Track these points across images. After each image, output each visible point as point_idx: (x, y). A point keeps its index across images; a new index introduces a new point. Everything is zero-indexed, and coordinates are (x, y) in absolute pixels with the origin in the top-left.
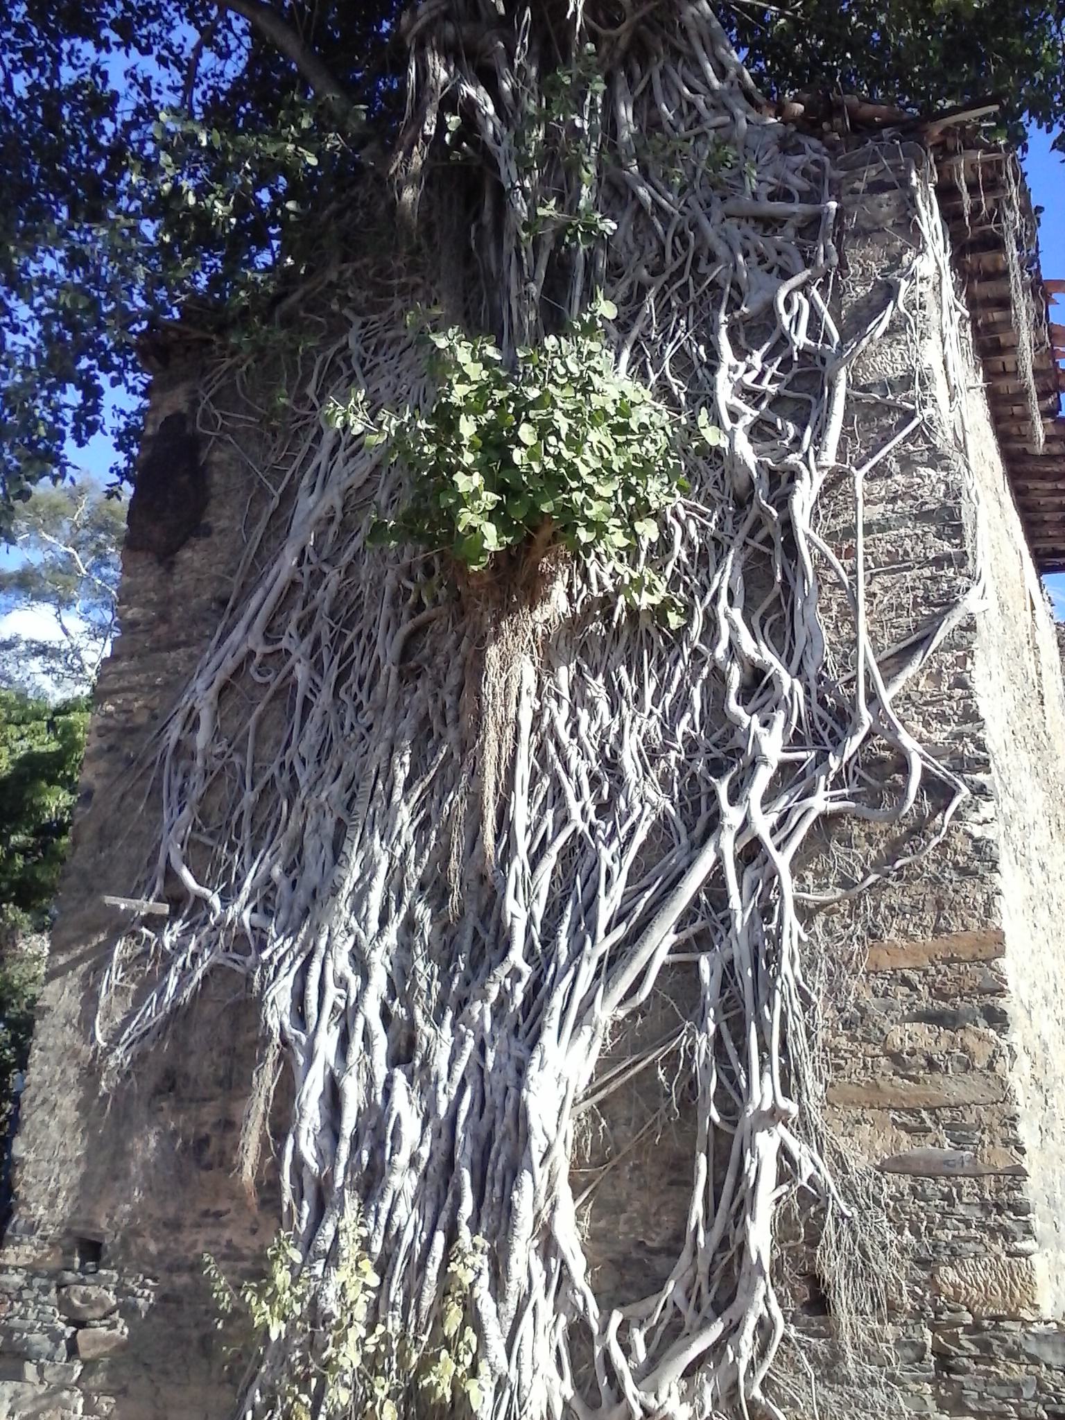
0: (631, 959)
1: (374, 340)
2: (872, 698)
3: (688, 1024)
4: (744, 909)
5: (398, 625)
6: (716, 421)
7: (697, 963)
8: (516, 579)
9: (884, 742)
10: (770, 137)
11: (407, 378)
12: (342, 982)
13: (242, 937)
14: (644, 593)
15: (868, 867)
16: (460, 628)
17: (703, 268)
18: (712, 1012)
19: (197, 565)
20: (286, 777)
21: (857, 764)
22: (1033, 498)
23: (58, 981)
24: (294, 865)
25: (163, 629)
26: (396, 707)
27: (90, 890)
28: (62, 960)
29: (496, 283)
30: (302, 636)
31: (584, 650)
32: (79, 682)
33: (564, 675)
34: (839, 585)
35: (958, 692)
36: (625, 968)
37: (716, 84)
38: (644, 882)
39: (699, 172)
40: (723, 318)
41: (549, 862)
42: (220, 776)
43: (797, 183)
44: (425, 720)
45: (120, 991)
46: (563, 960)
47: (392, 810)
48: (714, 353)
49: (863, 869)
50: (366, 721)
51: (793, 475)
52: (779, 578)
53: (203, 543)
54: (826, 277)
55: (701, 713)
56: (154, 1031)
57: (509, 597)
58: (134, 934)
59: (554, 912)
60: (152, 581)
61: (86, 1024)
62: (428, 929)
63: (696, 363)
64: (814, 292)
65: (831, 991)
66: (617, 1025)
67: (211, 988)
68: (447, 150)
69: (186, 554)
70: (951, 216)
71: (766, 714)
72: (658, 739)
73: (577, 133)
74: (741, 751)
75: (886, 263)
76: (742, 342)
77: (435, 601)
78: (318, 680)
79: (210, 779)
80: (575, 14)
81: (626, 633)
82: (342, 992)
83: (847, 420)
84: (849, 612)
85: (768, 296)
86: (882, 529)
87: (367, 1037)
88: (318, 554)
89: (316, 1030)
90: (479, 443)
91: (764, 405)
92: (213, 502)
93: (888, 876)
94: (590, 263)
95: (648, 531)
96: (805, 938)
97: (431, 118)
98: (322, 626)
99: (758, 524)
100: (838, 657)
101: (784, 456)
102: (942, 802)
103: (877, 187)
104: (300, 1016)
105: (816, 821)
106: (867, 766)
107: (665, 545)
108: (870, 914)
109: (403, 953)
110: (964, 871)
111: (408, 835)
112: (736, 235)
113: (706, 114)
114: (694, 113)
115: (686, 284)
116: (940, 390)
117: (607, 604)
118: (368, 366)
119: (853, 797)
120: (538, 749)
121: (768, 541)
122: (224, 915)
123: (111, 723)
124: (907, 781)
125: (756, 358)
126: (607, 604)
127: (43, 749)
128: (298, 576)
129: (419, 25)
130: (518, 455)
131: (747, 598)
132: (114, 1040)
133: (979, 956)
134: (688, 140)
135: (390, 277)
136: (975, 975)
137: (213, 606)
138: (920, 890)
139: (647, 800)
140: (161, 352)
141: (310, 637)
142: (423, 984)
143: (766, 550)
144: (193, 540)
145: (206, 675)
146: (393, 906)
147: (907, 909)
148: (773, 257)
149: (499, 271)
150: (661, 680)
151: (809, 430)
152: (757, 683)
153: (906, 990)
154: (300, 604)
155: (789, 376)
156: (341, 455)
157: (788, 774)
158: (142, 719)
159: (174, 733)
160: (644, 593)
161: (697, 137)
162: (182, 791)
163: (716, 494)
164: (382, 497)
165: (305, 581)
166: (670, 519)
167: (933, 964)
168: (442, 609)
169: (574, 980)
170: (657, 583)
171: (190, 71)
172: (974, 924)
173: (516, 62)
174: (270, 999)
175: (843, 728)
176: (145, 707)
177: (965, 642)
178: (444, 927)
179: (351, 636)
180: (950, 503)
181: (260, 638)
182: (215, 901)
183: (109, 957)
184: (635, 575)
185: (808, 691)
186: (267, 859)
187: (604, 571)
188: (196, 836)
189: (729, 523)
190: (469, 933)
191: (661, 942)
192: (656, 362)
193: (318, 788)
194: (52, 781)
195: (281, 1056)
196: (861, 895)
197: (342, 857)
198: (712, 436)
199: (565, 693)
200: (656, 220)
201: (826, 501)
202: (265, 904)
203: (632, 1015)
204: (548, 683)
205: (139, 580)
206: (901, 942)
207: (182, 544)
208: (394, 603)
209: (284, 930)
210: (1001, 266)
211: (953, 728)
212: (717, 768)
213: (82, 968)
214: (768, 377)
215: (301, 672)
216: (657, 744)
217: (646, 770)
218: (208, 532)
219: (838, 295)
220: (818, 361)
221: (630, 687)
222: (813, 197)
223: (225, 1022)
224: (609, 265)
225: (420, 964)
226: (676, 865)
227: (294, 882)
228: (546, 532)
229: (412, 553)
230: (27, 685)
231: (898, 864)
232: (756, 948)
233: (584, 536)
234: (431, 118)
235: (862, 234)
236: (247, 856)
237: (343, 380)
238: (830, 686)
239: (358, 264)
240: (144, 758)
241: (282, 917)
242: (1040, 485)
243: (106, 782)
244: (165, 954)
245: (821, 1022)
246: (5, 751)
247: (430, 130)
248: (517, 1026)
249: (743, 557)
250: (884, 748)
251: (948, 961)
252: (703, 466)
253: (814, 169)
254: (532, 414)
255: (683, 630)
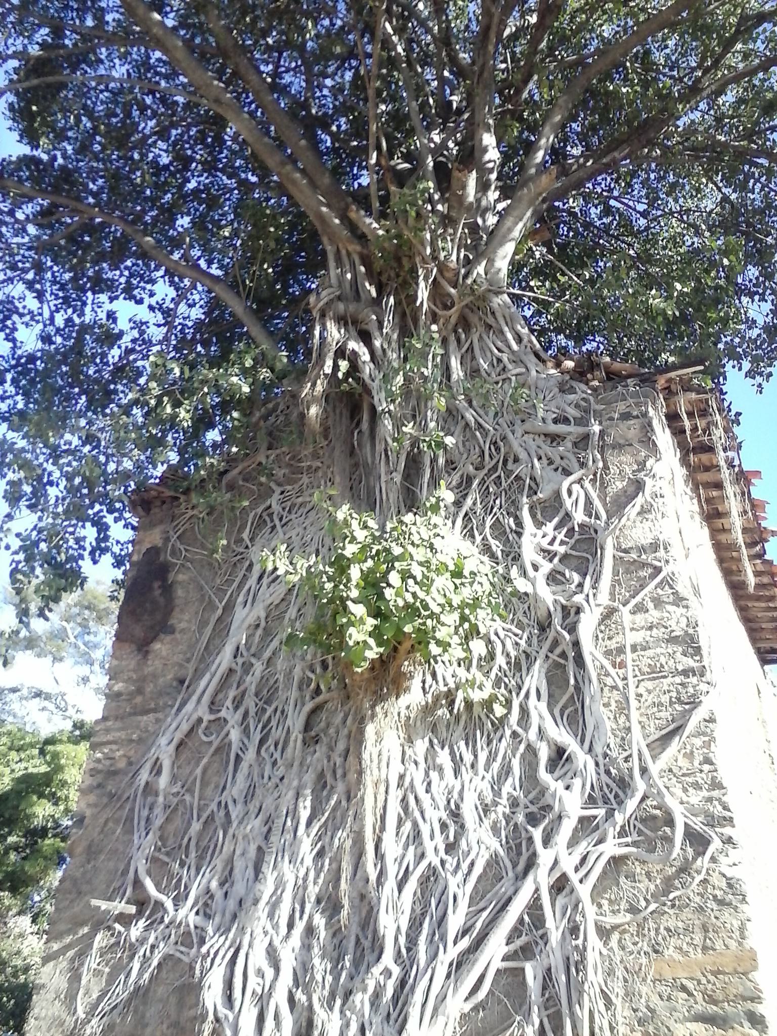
0: (473, 965)
1: (289, 503)
2: (644, 771)
3: (518, 1018)
4: (557, 928)
5: (303, 704)
6: (524, 574)
7: (523, 969)
8: (386, 677)
9: (655, 803)
10: (553, 382)
11: (311, 530)
12: (260, 973)
13: (188, 934)
14: (476, 689)
15: (649, 897)
16: (346, 708)
17: (510, 466)
18: (536, 1009)
19: (164, 653)
20: (222, 813)
21: (636, 819)
22: (753, 613)
23: (52, 964)
24: (226, 880)
25: (139, 699)
26: (301, 764)
27: (80, 893)
28: (56, 946)
29: (370, 470)
30: (236, 708)
31: (434, 729)
32: (65, 718)
33: (421, 746)
34: (615, 688)
35: (706, 767)
36: (469, 971)
37: (515, 347)
38: (482, 905)
39: (506, 404)
40: (525, 500)
41: (412, 885)
42: (176, 809)
43: (572, 412)
44: (321, 775)
45: (97, 973)
46: (422, 963)
47: (297, 842)
48: (519, 523)
49: (645, 899)
50: (280, 773)
51: (578, 610)
52: (572, 682)
53: (168, 638)
54: (595, 475)
55: (521, 778)
56: (121, 1006)
57: (382, 690)
58: (109, 928)
59: (415, 924)
60: (133, 664)
61: (70, 998)
62: (323, 934)
63: (508, 530)
64: (587, 484)
65: (627, 995)
66: (463, 1016)
67: (164, 974)
68: (339, 382)
69: (157, 646)
70: (678, 432)
71: (567, 780)
72: (489, 797)
73: (425, 379)
74: (549, 808)
75: (635, 467)
76: (539, 516)
77: (329, 689)
78: (246, 741)
79: (169, 811)
80: (422, 303)
81: (464, 718)
82: (260, 981)
83: (615, 573)
84: (623, 708)
85: (556, 487)
86: (644, 649)
87: (277, 1017)
88: (248, 650)
89: (240, 1011)
90: (362, 584)
91: (556, 560)
92: (177, 610)
93: (664, 905)
94: (434, 460)
95: (478, 647)
96: (605, 952)
97: (329, 363)
98: (250, 702)
99: (556, 643)
100: (618, 740)
101: (572, 596)
102: (701, 849)
103: (626, 416)
104: (229, 999)
105: (609, 862)
106: (643, 821)
107: (491, 656)
108: (653, 933)
109: (304, 952)
110: (721, 902)
111: (309, 861)
112: (532, 446)
113: (510, 366)
114: (502, 365)
115: (499, 477)
116: (676, 551)
117: (450, 697)
118: (284, 521)
119: (635, 844)
120: (403, 800)
121: (563, 655)
122: (176, 916)
123: (100, 767)
124: (673, 832)
125: (549, 527)
126: (450, 697)
127: (35, 771)
128: (234, 665)
129: (322, 303)
130: (389, 593)
131: (550, 696)
132: (90, 1013)
133: (740, 970)
134: (497, 383)
135: (300, 461)
136: (737, 986)
137: (175, 684)
138: (690, 916)
139: (483, 842)
140: (146, 503)
141: (241, 710)
142: (319, 977)
143: (562, 661)
144: (162, 636)
145: (168, 735)
146: (297, 915)
147: (681, 931)
148: (558, 461)
149: (373, 462)
150: (490, 752)
151: (588, 578)
152: (559, 755)
153: (684, 996)
154: (235, 685)
155: (573, 541)
156: (265, 581)
157: (586, 825)
158: (122, 764)
159: (144, 776)
160: (476, 689)
161: (504, 380)
162: (148, 819)
163: (525, 621)
164: (292, 612)
165: (238, 668)
166: (493, 637)
167: (704, 976)
168: (334, 694)
169: (431, 980)
170: (485, 683)
171: (168, 314)
172: (733, 944)
173: (385, 331)
174: (207, 985)
175: (625, 793)
176: (124, 756)
177: (708, 730)
178: (336, 932)
179: (270, 710)
180: (691, 631)
181: (206, 709)
182: (169, 904)
183: (90, 946)
184: (470, 677)
185: (597, 764)
186: (207, 874)
187: (448, 672)
188: (157, 854)
189: (535, 640)
190: (353, 939)
191: (496, 949)
192: (480, 528)
193: (245, 822)
194: (41, 796)
195: (214, 1030)
196: (645, 919)
197: (261, 876)
198: (522, 585)
199: (421, 760)
200: (478, 433)
201: (603, 628)
202: (205, 910)
203: (475, 1009)
204: (409, 752)
205: (124, 663)
206: (677, 956)
207: (154, 638)
208: (300, 688)
209: (218, 929)
210: (715, 463)
211: (705, 793)
212: (533, 820)
213: (71, 953)
214: (558, 541)
215: (235, 735)
216: (488, 800)
217: (481, 819)
218: (172, 631)
219: (603, 487)
220: (592, 531)
221: (468, 757)
222: (582, 422)
223: (173, 1000)
224: (447, 461)
225: (316, 961)
226: (505, 893)
227: (226, 893)
228: (407, 645)
229: (310, 652)
230: (26, 719)
231: (671, 896)
232: (568, 959)
233: (434, 649)
234: (329, 363)
235: (618, 447)
236: (193, 871)
237: (267, 529)
238: (613, 761)
239: (278, 451)
240: (124, 792)
241: (217, 919)
242: (756, 604)
243: (95, 811)
244: (132, 945)
245: (620, 1020)
246: (7, 771)
247: (328, 369)
248: (389, 1014)
249: (546, 666)
250: (655, 808)
251: (716, 973)
252: (514, 604)
253: (583, 403)
254: (397, 564)
255: (503, 720)
